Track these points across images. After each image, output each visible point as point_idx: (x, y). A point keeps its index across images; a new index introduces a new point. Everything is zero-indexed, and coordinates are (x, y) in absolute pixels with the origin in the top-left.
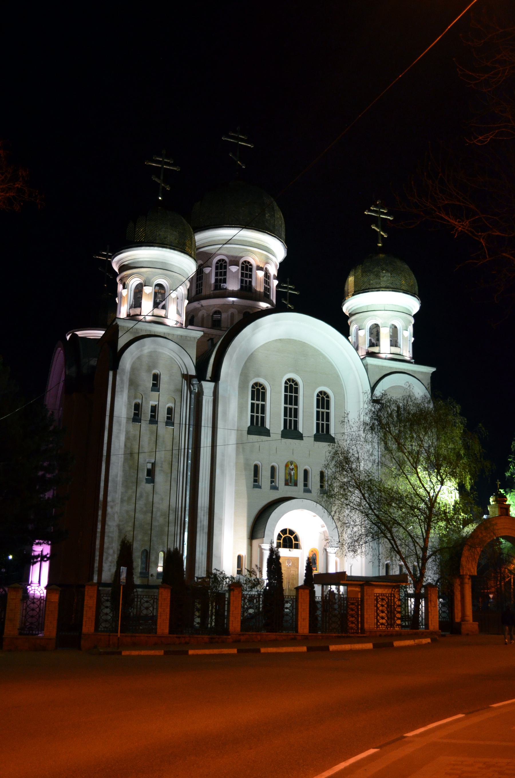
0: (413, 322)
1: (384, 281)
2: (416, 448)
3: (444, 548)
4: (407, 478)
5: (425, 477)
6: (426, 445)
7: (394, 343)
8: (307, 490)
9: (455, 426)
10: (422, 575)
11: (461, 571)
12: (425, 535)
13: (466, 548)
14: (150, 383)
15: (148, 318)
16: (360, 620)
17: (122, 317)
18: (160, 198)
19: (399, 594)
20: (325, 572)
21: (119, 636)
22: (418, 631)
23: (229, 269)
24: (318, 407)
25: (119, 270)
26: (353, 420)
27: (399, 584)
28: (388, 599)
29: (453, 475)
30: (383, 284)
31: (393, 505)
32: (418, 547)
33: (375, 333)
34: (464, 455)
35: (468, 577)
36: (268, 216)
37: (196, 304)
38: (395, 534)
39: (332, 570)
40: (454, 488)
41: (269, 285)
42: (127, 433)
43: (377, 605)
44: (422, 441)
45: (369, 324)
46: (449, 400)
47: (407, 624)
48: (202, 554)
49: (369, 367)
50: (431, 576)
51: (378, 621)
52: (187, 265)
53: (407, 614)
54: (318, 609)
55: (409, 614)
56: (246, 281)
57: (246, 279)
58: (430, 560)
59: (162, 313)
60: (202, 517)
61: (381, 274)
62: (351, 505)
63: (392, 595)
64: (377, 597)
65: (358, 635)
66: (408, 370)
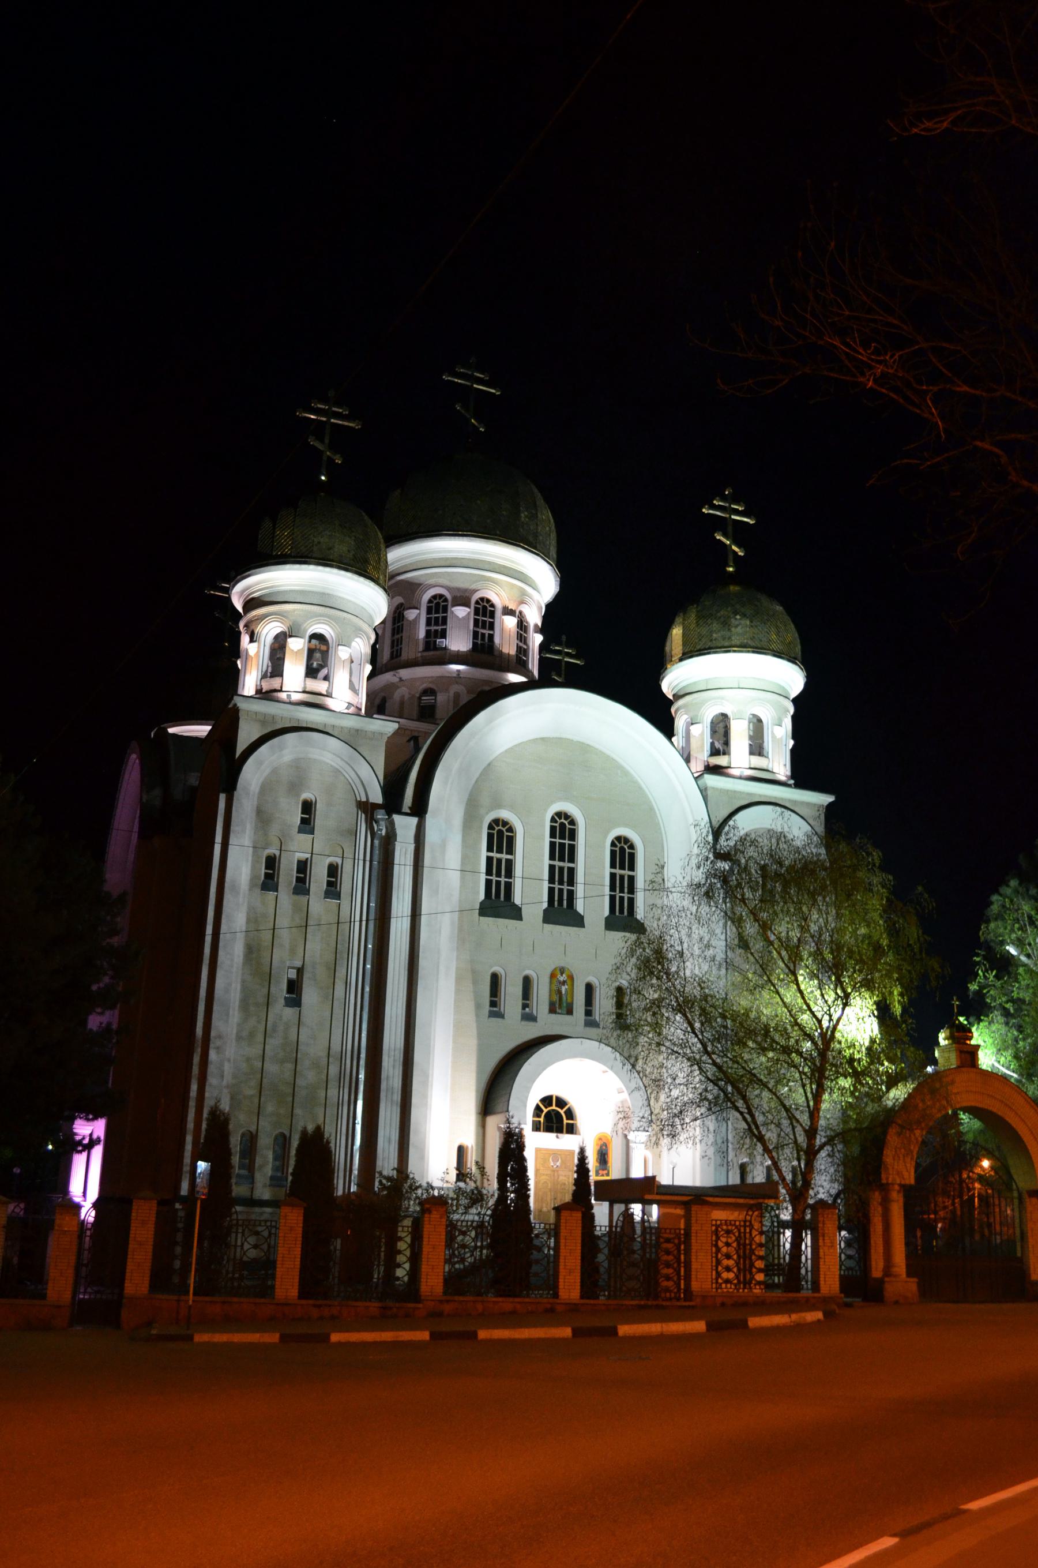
0: (792, 710)
1: (738, 634)
2: (795, 934)
3: (850, 1130)
4: (778, 992)
5: (812, 992)
6: (814, 928)
7: (757, 748)
8: (591, 1022)
9: (871, 890)
10: (807, 1184)
11: (883, 1176)
12: (811, 1103)
13: (892, 1131)
14: (296, 817)
15: (296, 697)
16: (682, 1273)
17: (246, 693)
18: (323, 478)
19: (761, 1222)
20: (624, 1177)
21: (191, 1303)
22: (798, 1295)
23: (452, 612)
24: (613, 865)
25: (244, 608)
26: (673, 880)
27: (761, 1201)
28: (739, 1231)
29: (868, 985)
30: (736, 640)
31: (750, 1044)
32: (799, 1130)
33: (722, 731)
34: (888, 946)
35: (897, 1187)
36: (526, 517)
37: (388, 677)
38: (756, 1102)
39: (637, 1172)
40: (868, 1012)
41: (525, 643)
42: (251, 910)
43: (717, 1242)
44: (805, 920)
45: (709, 714)
46: (858, 840)
47: (776, 1280)
48: (389, 1142)
49: (709, 792)
50: (824, 1185)
51: (719, 1275)
52: (370, 601)
53: (776, 1261)
54: (599, 1251)
55: (782, 1261)
56: (483, 635)
57: (484, 631)
58: (823, 1153)
59: (321, 686)
60: (391, 1070)
61: (733, 620)
62: (667, 1044)
63: (748, 1224)
64: (717, 1227)
65: (678, 1304)
66: (782, 799)
